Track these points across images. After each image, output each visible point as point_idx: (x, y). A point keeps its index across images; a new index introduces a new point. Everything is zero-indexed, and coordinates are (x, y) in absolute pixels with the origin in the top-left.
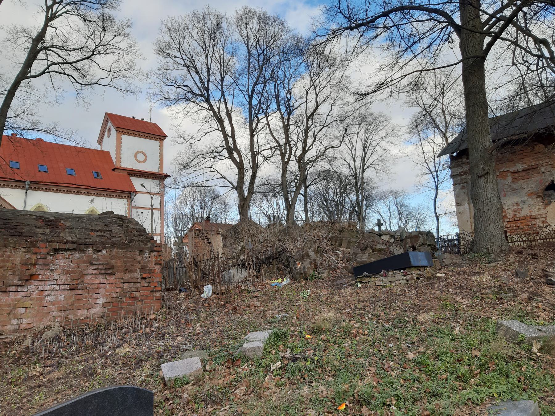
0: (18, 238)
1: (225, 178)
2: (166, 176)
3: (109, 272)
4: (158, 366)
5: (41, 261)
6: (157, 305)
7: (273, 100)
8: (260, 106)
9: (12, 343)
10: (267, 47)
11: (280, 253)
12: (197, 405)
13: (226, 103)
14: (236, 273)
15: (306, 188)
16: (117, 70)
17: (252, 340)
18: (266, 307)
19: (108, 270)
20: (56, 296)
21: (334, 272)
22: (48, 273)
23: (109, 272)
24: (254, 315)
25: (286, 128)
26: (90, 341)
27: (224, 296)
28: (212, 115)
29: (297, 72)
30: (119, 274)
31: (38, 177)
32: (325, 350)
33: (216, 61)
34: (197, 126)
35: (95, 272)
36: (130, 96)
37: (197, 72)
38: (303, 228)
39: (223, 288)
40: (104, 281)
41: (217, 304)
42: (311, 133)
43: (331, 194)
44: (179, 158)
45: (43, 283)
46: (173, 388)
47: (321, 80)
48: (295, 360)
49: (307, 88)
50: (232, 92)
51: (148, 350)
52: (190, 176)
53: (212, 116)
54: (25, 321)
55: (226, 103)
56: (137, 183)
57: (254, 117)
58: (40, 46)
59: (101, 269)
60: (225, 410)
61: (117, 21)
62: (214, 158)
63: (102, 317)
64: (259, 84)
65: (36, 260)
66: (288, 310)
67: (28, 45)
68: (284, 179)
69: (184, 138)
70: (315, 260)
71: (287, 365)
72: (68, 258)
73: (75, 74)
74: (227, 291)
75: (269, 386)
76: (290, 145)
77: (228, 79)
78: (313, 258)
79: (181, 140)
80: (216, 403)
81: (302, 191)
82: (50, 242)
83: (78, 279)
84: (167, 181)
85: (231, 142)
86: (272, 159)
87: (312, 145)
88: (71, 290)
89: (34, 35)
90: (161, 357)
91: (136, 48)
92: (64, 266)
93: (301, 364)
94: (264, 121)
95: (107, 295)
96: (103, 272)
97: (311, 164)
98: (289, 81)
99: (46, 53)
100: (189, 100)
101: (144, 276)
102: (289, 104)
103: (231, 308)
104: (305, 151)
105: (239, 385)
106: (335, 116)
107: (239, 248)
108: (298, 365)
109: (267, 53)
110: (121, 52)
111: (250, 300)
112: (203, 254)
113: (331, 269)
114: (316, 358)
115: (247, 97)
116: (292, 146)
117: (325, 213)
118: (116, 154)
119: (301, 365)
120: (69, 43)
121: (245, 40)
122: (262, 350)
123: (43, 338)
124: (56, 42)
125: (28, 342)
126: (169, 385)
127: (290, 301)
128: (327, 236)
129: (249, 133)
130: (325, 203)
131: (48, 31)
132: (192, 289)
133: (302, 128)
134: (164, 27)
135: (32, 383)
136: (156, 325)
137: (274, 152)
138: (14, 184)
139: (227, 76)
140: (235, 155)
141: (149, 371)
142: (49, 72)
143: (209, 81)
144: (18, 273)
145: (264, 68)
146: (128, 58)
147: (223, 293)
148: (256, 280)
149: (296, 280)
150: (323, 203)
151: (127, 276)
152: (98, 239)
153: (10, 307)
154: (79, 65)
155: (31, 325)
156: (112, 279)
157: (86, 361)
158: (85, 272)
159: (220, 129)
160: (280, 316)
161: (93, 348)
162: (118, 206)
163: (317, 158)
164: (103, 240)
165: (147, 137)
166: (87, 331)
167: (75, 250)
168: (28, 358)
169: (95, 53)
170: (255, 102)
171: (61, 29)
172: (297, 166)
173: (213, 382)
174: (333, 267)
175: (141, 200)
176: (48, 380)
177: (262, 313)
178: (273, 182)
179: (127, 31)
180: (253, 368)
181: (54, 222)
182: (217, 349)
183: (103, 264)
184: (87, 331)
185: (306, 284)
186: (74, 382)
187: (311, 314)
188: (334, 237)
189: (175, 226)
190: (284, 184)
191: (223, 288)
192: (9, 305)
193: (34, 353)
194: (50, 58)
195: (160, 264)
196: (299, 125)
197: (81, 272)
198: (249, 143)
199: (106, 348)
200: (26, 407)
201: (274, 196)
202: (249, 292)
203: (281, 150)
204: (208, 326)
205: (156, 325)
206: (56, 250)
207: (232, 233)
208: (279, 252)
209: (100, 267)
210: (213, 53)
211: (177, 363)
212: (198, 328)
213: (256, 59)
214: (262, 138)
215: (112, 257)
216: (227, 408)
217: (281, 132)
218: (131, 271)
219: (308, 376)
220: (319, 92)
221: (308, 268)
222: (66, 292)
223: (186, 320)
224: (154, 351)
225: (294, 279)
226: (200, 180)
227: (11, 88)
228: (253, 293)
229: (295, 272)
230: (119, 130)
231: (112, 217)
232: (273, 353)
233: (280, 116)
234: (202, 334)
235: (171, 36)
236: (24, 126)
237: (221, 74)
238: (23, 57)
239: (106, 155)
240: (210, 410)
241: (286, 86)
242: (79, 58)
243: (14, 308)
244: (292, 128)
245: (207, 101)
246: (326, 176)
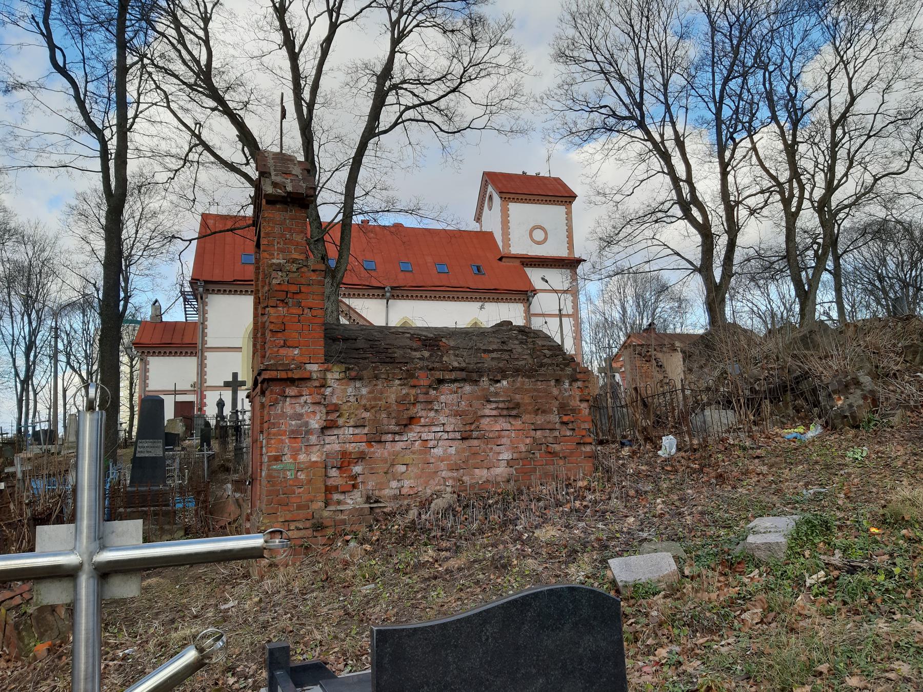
0: (391, 366)
1: (678, 255)
2: (579, 261)
3: (514, 413)
4: (604, 562)
5: (421, 398)
6: (588, 466)
7: (761, 104)
8: (737, 117)
9: (393, 514)
10: (745, 8)
11: (798, 380)
12: (676, 631)
14: (716, 416)
15: (837, 258)
16: (497, 100)
17: (762, 531)
18: (779, 476)
19: (512, 410)
20: (445, 449)
21: (915, 414)
22: (432, 414)
23: (514, 413)
24: (758, 489)
25: (791, 150)
26: (496, 517)
27: (699, 456)
28: (651, 147)
29: (805, 44)
30: (528, 416)
31: (401, 280)
32: (915, 557)
33: (654, 53)
34: (626, 171)
35: (494, 413)
36: (519, 140)
37: (622, 79)
38: (841, 332)
39: (695, 442)
40: (507, 426)
41: (688, 467)
42: (842, 153)
43: (892, 265)
44: (598, 230)
45: (426, 429)
46: (632, 598)
47: (857, 48)
48: (852, 570)
49: (828, 69)
50: (683, 102)
51: (582, 535)
52: (618, 257)
53: (651, 151)
54: (407, 483)
56: (535, 276)
57: (727, 140)
58: (388, 84)
59: (502, 409)
60: (729, 644)
61: (490, 21)
62: (656, 222)
63: (508, 481)
64: (734, 78)
65: (416, 397)
66: (824, 482)
67: (373, 86)
68: (791, 245)
69: (605, 195)
70: (872, 392)
71: (837, 578)
72: (456, 392)
73: (438, 119)
74: (704, 446)
75: (806, 612)
76: (800, 182)
77: (677, 81)
78: (869, 388)
79: (600, 198)
80: (711, 632)
81: (830, 264)
82: (431, 370)
83: (471, 424)
84: (580, 269)
86: (765, 212)
87: (846, 175)
88: (463, 439)
89: (379, 69)
90: (605, 550)
91: (523, 59)
92: (452, 405)
93: (867, 579)
94: (747, 143)
95: (513, 448)
96: (505, 413)
97: (847, 210)
98: (791, 63)
99: (397, 94)
100: (611, 130)
101: (565, 419)
102: (794, 105)
103: (713, 474)
104: (831, 188)
105: (749, 605)
106: (892, 112)
107: (716, 373)
108: (860, 581)
109: (745, 19)
110: (501, 71)
111: (746, 462)
112: (649, 387)
113: (907, 407)
114: (897, 571)
115: (712, 106)
116: (804, 182)
117: (879, 303)
119: (866, 581)
120: (426, 72)
121: (704, 5)
122: (784, 549)
123: (432, 509)
124: (410, 74)
125: (413, 514)
126: (626, 593)
127: (827, 467)
128: (894, 345)
129: (718, 169)
130: (878, 285)
131: (396, 60)
132: (642, 442)
133: (823, 146)
134: (565, 14)
135: (425, 573)
136: (590, 497)
137: (769, 198)
138: (371, 292)
139: (674, 75)
140: (695, 212)
141: (589, 569)
142: (403, 122)
143: (642, 90)
144: (393, 415)
145: (742, 49)
146: (511, 79)
147: (695, 450)
148: (754, 428)
149: (834, 428)
150: (874, 285)
151: (540, 420)
152: (494, 363)
153: (386, 463)
154: (442, 104)
155: (415, 490)
156: (518, 423)
157: (494, 545)
158: (480, 413)
159: (666, 170)
160: (811, 491)
161: (500, 527)
162: (514, 313)
163: (858, 199)
164: (501, 365)
166: (491, 502)
167: (464, 380)
168: (416, 536)
169: (463, 80)
170: (727, 113)
171: (413, 53)
172: (818, 219)
173: (699, 595)
174: (912, 403)
175: (544, 302)
176: (446, 570)
177: (774, 486)
178: (769, 253)
179: (507, 35)
180: (771, 578)
181: (432, 341)
182: (698, 542)
183: (503, 401)
184: (491, 502)
185: (856, 436)
186: (481, 576)
187: (874, 490)
188: (911, 346)
189: (597, 341)
190: (791, 256)
191: (695, 442)
192: (385, 461)
193: (424, 530)
194: (402, 101)
195: (588, 401)
196: (816, 141)
197: (476, 413)
198: (719, 187)
199: (519, 528)
200: (422, 606)
201: (773, 278)
202: (745, 449)
203: (781, 193)
204: (677, 503)
205: (590, 497)
206: (441, 382)
207: (700, 349)
208: (796, 378)
209: (501, 405)
210: (648, 40)
211: (634, 560)
212: (660, 506)
213: (725, 36)
214: (744, 176)
215: (517, 391)
216: (730, 640)
217: (780, 159)
218: (544, 412)
219: (884, 600)
220: (855, 72)
221: (859, 407)
222: (457, 442)
223: (637, 491)
224: (593, 537)
225: (830, 427)
226: (636, 261)
228: (750, 451)
229: (832, 414)
230: (504, 196)
231: (511, 330)
232: (807, 556)
233: (777, 130)
234: (667, 516)
235: (576, 27)
236: (377, 208)
237: (663, 74)
238: (366, 105)
239: (488, 237)
240: (701, 641)
241: (787, 73)
242: (442, 93)
243: (393, 465)
244: (802, 148)
245: (642, 125)
246: (880, 231)
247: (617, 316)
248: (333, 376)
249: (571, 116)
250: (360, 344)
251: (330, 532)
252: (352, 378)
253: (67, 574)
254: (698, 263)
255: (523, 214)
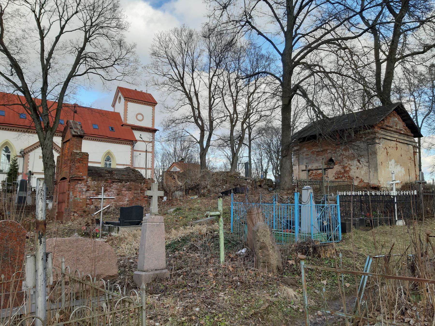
6: (146, 202)
13: (194, 86)
19: (129, 189)
40: (128, 193)
55: (194, 86)
56: (137, 134)
85: (197, 112)
118: (124, 115)
151: (136, 192)
165: (144, 104)
206: (113, 182)
215: (131, 185)
227: (66, 80)
230: (126, 99)
245: (183, 85)
247: (172, 151)
248: (89, 179)
249: (156, 76)
250: (93, 171)
251: (87, 213)
252: (93, 180)
253: (101, 199)
254: (199, 140)
255: (134, 108)
